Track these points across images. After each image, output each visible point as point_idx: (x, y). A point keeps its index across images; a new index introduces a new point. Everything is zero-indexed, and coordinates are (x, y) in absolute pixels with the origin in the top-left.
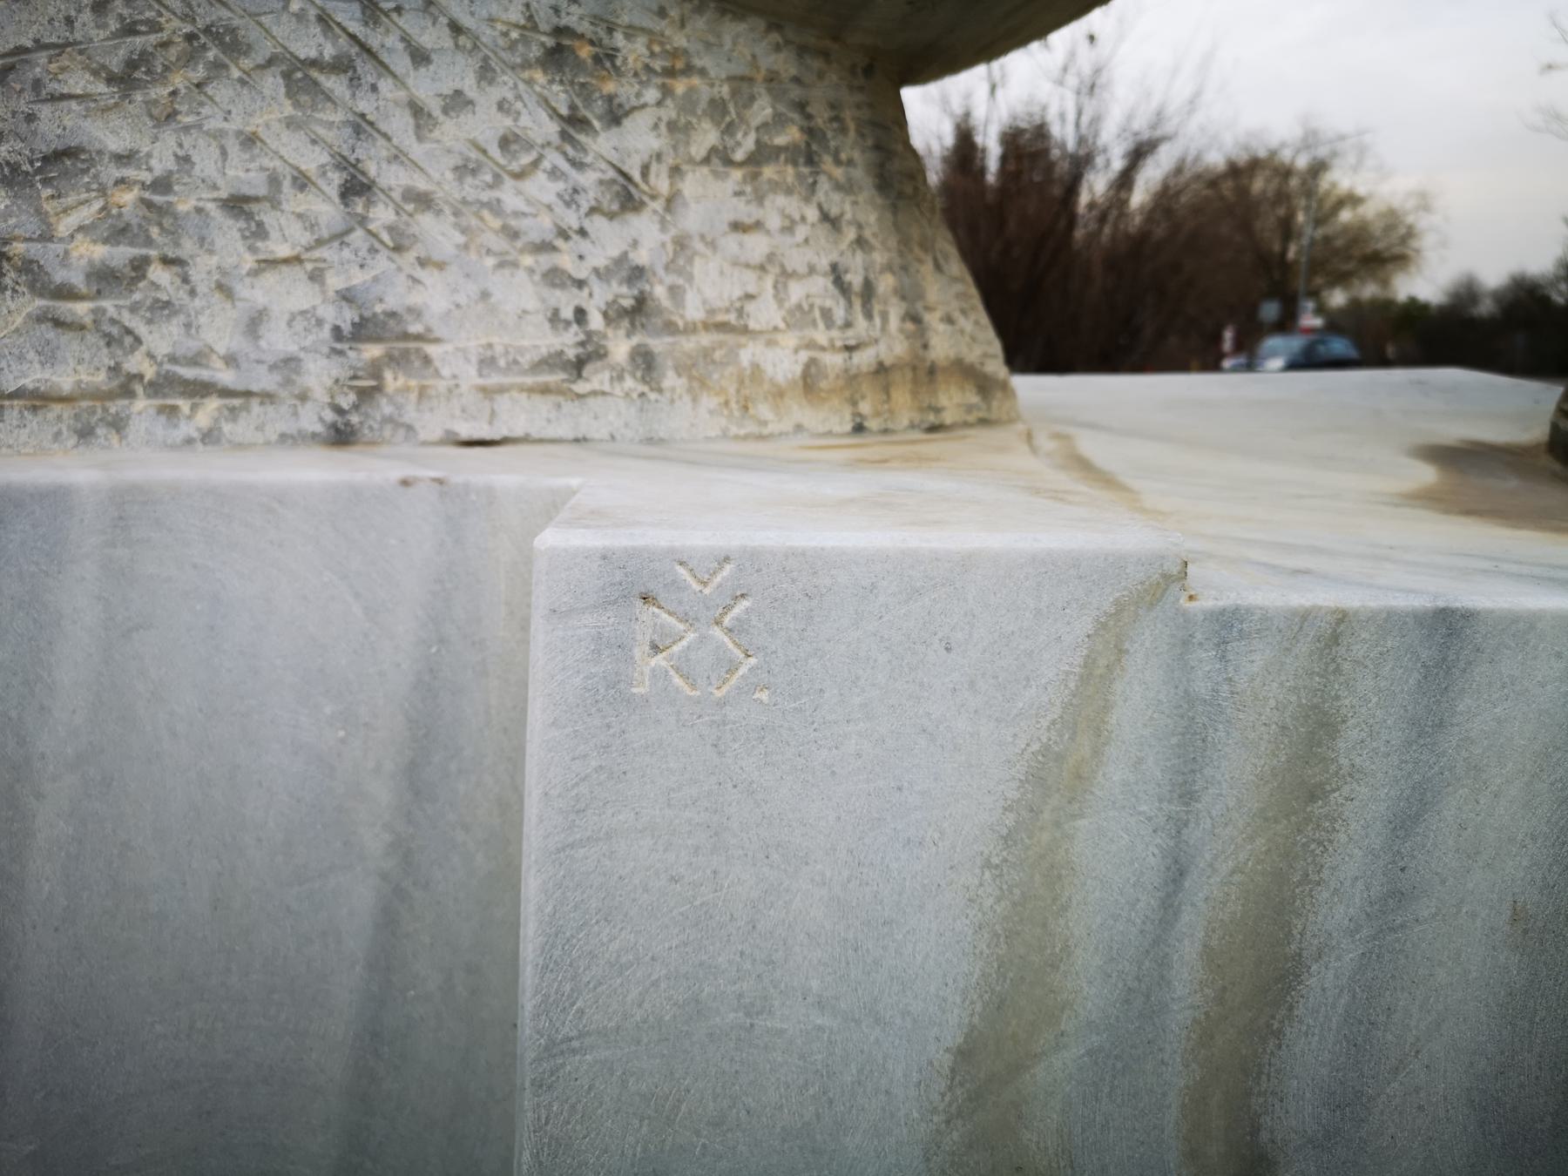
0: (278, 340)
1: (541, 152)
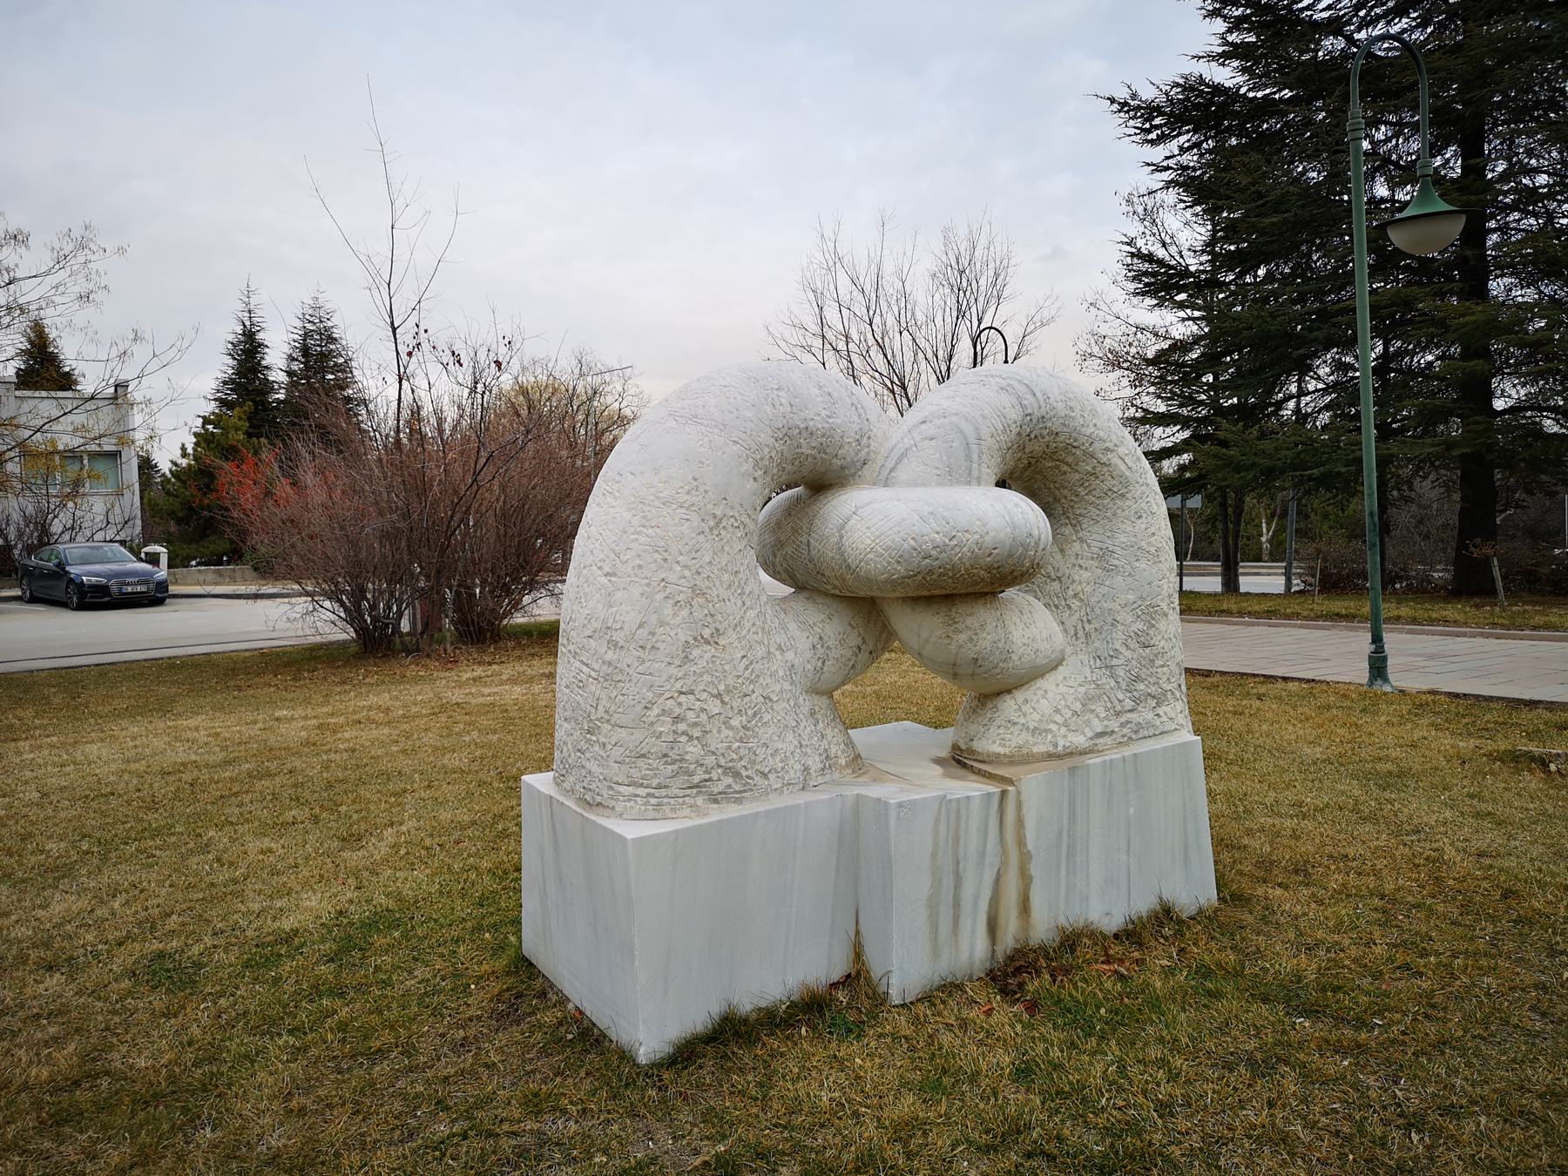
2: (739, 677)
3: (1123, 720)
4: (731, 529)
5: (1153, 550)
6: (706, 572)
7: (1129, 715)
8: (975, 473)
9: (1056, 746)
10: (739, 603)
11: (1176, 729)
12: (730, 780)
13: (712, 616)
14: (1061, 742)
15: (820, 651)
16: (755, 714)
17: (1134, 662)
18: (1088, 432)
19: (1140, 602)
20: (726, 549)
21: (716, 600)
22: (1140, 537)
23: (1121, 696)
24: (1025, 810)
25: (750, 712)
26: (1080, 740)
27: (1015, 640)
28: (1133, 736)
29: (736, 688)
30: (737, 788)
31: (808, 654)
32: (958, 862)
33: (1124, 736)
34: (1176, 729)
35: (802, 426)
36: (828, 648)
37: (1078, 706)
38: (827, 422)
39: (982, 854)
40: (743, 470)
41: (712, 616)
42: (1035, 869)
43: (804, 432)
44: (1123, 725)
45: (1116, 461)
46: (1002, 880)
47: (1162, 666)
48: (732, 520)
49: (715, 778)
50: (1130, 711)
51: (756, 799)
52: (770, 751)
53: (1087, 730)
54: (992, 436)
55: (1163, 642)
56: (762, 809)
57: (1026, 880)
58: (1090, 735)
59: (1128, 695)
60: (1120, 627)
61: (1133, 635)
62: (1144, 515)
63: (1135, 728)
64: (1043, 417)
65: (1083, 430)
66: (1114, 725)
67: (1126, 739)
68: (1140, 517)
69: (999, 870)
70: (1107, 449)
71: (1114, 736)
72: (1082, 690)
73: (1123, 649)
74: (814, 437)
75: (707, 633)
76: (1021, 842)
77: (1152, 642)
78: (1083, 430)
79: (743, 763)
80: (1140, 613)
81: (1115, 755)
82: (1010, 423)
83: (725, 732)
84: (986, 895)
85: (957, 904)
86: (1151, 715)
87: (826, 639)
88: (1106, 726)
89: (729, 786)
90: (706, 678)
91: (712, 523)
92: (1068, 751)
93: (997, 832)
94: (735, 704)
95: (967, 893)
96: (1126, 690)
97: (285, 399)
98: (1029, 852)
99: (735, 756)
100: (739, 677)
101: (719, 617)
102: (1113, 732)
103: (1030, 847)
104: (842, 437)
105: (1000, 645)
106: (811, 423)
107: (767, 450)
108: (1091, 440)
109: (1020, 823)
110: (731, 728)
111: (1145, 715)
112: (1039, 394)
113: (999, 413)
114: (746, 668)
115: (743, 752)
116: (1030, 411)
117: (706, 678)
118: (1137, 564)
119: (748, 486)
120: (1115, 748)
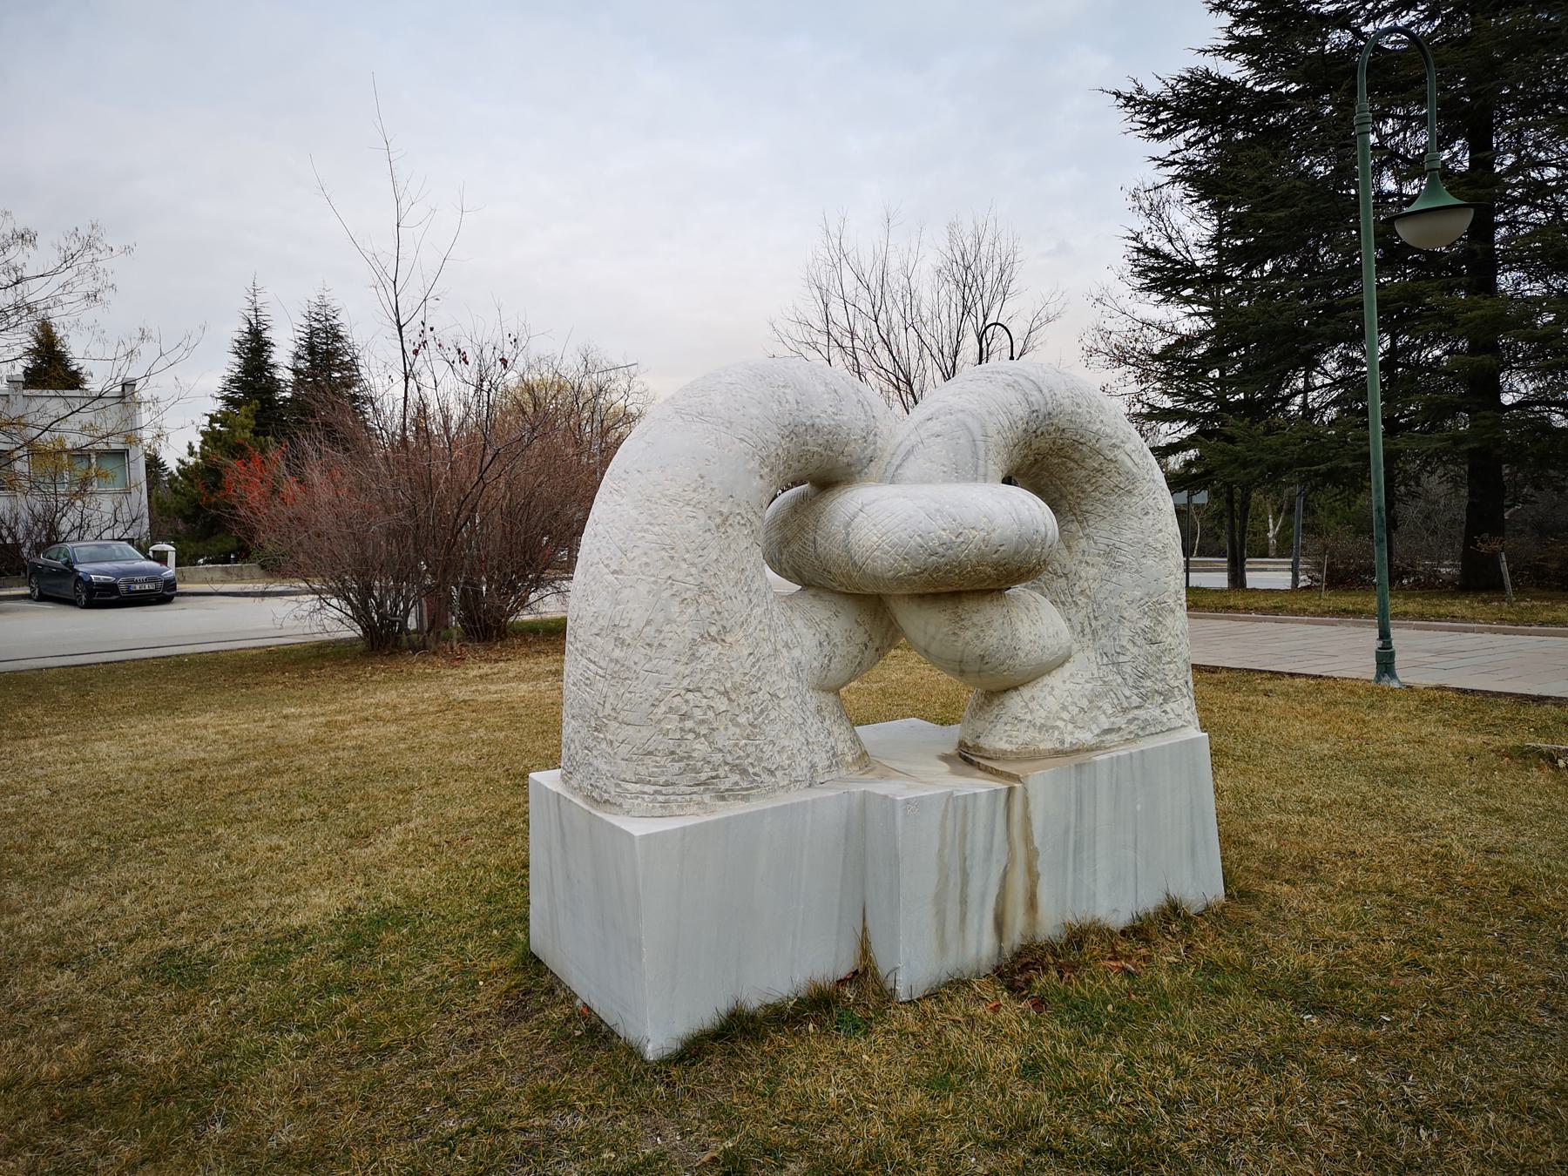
2: (745, 674)
3: (1130, 716)
4: (738, 527)
5: (1159, 546)
7: (1136, 712)
8: (981, 470)
9: (1062, 742)
11: (1183, 726)
13: (719, 613)
14: (1068, 739)
15: (827, 648)
16: (762, 711)
17: (1141, 659)
18: (1095, 429)
19: (1147, 599)
21: (722, 597)
22: (1147, 533)
23: (1128, 693)
24: (1032, 807)
25: (757, 710)
26: (1087, 737)
27: (1021, 637)
28: (1140, 733)
29: (743, 686)
30: (744, 785)
31: (815, 652)
32: (965, 860)
33: (1130, 733)
34: (1183, 726)
35: (808, 423)
36: (835, 645)
37: (1085, 703)
38: (834, 420)
39: (989, 851)
41: (719, 613)
42: (1041, 866)
43: (810, 429)
44: (1130, 722)
45: (1122, 457)
46: (1008, 877)
47: (1169, 663)
48: (739, 517)
49: (722, 775)
50: (1137, 708)
52: (777, 748)
53: (1094, 727)
55: (1170, 639)
56: (770, 806)
57: (1033, 876)
58: (1097, 731)
59: (1135, 691)
61: (1139, 631)
62: (1151, 512)
63: (1142, 725)
64: (1049, 414)
65: (1090, 426)
66: (1121, 721)
67: (1133, 736)
68: (1147, 513)
70: (1114, 446)
72: (1089, 686)
73: (1129, 646)
74: (821, 434)
76: (1028, 838)
77: (1159, 639)
78: (1090, 426)
81: (1123, 752)
82: (1016, 419)
83: (732, 729)
84: (993, 891)
86: (1158, 711)
87: (832, 636)
88: (1113, 723)
89: (736, 783)
90: (713, 675)
92: (1075, 747)
93: (1005, 828)
94: (742, 702)
99: (742, 753)
100: (745, 674)
101: (726, 614)
102: (1120, 729)
104: (848, 434)
105: (1007, 642)
106: (817, 420)
107: (773, 448)
108: (1097, 437)
109: (1027, 819)
110: (738, 725)
113: (1005, 410)
114: (753, 666)
115: (750, 749)
118: (1144, 561)
119: (755, 484)
120: (1122, 745)
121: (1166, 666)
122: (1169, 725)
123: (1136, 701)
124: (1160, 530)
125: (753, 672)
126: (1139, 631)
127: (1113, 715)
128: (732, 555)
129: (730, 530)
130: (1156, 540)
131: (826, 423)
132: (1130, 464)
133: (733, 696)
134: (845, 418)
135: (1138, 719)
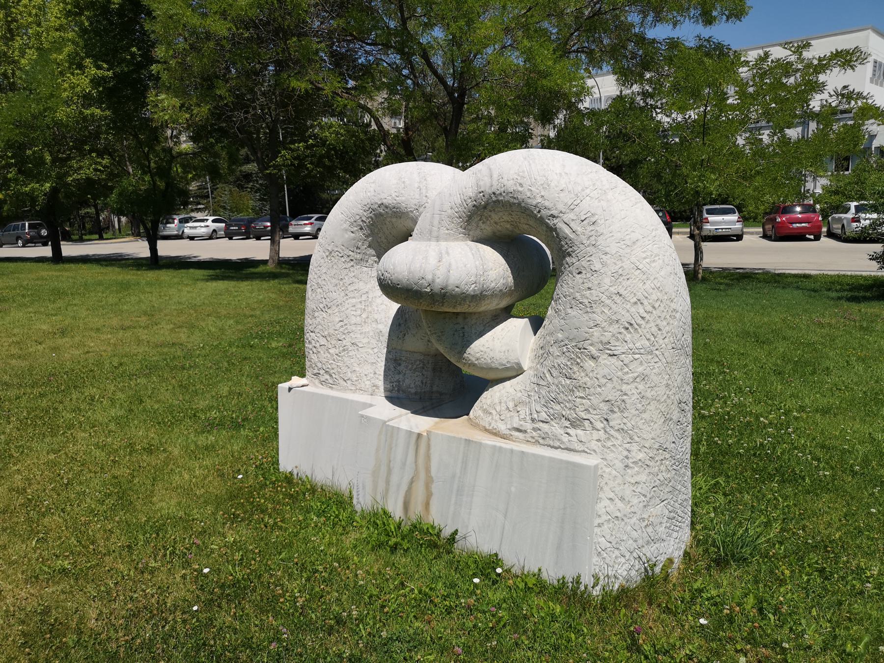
0: (367, 387)
1: (617, 508)
2: (336, 330)
3: (535, 426)
5: (586, 301)
6: (324, 277)
7: (541, 424)
8: (435, 234)
9: (490, 424)
10: (343, 294)
12: (328, 377)
20: (335, 267)
22: (576, 289)
23: (538, 409)
24: (432, 451)
26: (502, 428)
32: (390, 461)
33: (533, 438)
35: (379, 203)
37: (511, 405)
39: (404, 464)
40: (342, 227)
42: (434, 488)
44: (534, 429)
45: (561, 225)
50: (543, 422)
51: (338, 390)
53: (509, 422)
54: (452, 208)
57: (429, 495)
58: (509, 426)
59: (546, 410)
60: (551, 357)
61: (556, 366)
62: (584, 272)
66: (528, 426)
68: (580, 273)
69: (413, 478)
71: (526, 435)
72: (519, 394)
75: (321, 306)
76: (428, 470)
79: (333, 371)
80: (565, 350)
82: (466, 198)
85: (388, 482)
86: (562, 431)
90: (320, 327)
91: (327, 254)
92: (494, 431)
95: (395, 479)
96: (544, 405)
97: (807, 101)
98: (432, 478)
100: (336, 330)
101: (328, 300)
102: (525, 432)
103: (433, 473)
107: (358, 217)
109: (428, 457)
111: (556, 428)
112: (495, 176)
113: (461, 192)
114: (342, 326)
115: (334, 366)
116: (482, 189)
117: (320, 327)
118: (569, 311)
121: (578, 400)
122: (568, 445)
123: (544, 416)
124: (589, 288)
125: (341, 330)
126: (556, 366)
127: (524, 419)
128: (334, 271)
129: (333, 258)
130: (583, 296)
131: (390, 202)
132: (567, 231)
133: (329, 339)
134: (403, 198)
135: (540, 430)
